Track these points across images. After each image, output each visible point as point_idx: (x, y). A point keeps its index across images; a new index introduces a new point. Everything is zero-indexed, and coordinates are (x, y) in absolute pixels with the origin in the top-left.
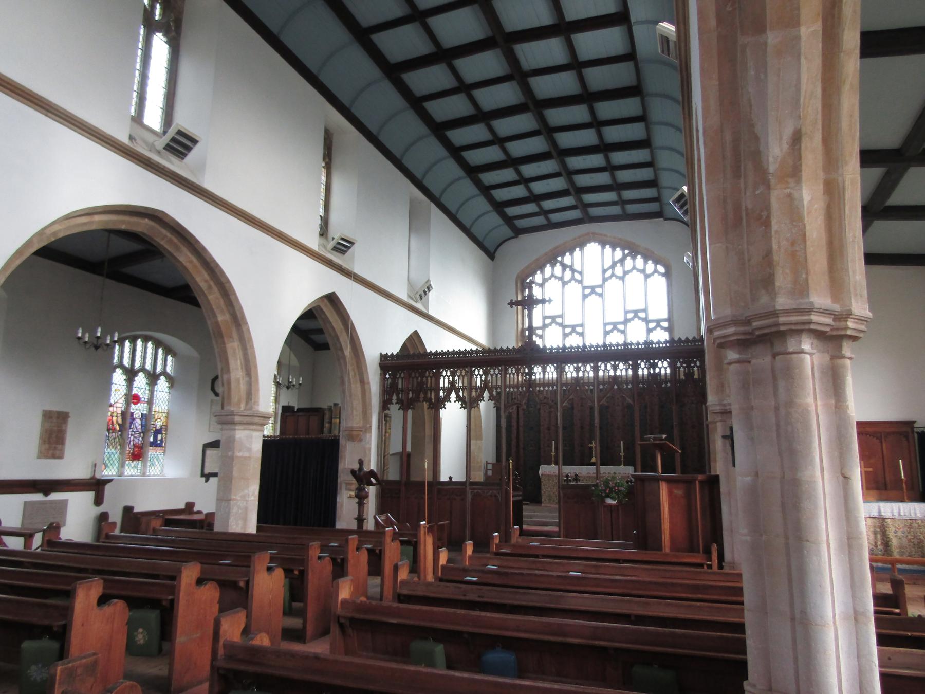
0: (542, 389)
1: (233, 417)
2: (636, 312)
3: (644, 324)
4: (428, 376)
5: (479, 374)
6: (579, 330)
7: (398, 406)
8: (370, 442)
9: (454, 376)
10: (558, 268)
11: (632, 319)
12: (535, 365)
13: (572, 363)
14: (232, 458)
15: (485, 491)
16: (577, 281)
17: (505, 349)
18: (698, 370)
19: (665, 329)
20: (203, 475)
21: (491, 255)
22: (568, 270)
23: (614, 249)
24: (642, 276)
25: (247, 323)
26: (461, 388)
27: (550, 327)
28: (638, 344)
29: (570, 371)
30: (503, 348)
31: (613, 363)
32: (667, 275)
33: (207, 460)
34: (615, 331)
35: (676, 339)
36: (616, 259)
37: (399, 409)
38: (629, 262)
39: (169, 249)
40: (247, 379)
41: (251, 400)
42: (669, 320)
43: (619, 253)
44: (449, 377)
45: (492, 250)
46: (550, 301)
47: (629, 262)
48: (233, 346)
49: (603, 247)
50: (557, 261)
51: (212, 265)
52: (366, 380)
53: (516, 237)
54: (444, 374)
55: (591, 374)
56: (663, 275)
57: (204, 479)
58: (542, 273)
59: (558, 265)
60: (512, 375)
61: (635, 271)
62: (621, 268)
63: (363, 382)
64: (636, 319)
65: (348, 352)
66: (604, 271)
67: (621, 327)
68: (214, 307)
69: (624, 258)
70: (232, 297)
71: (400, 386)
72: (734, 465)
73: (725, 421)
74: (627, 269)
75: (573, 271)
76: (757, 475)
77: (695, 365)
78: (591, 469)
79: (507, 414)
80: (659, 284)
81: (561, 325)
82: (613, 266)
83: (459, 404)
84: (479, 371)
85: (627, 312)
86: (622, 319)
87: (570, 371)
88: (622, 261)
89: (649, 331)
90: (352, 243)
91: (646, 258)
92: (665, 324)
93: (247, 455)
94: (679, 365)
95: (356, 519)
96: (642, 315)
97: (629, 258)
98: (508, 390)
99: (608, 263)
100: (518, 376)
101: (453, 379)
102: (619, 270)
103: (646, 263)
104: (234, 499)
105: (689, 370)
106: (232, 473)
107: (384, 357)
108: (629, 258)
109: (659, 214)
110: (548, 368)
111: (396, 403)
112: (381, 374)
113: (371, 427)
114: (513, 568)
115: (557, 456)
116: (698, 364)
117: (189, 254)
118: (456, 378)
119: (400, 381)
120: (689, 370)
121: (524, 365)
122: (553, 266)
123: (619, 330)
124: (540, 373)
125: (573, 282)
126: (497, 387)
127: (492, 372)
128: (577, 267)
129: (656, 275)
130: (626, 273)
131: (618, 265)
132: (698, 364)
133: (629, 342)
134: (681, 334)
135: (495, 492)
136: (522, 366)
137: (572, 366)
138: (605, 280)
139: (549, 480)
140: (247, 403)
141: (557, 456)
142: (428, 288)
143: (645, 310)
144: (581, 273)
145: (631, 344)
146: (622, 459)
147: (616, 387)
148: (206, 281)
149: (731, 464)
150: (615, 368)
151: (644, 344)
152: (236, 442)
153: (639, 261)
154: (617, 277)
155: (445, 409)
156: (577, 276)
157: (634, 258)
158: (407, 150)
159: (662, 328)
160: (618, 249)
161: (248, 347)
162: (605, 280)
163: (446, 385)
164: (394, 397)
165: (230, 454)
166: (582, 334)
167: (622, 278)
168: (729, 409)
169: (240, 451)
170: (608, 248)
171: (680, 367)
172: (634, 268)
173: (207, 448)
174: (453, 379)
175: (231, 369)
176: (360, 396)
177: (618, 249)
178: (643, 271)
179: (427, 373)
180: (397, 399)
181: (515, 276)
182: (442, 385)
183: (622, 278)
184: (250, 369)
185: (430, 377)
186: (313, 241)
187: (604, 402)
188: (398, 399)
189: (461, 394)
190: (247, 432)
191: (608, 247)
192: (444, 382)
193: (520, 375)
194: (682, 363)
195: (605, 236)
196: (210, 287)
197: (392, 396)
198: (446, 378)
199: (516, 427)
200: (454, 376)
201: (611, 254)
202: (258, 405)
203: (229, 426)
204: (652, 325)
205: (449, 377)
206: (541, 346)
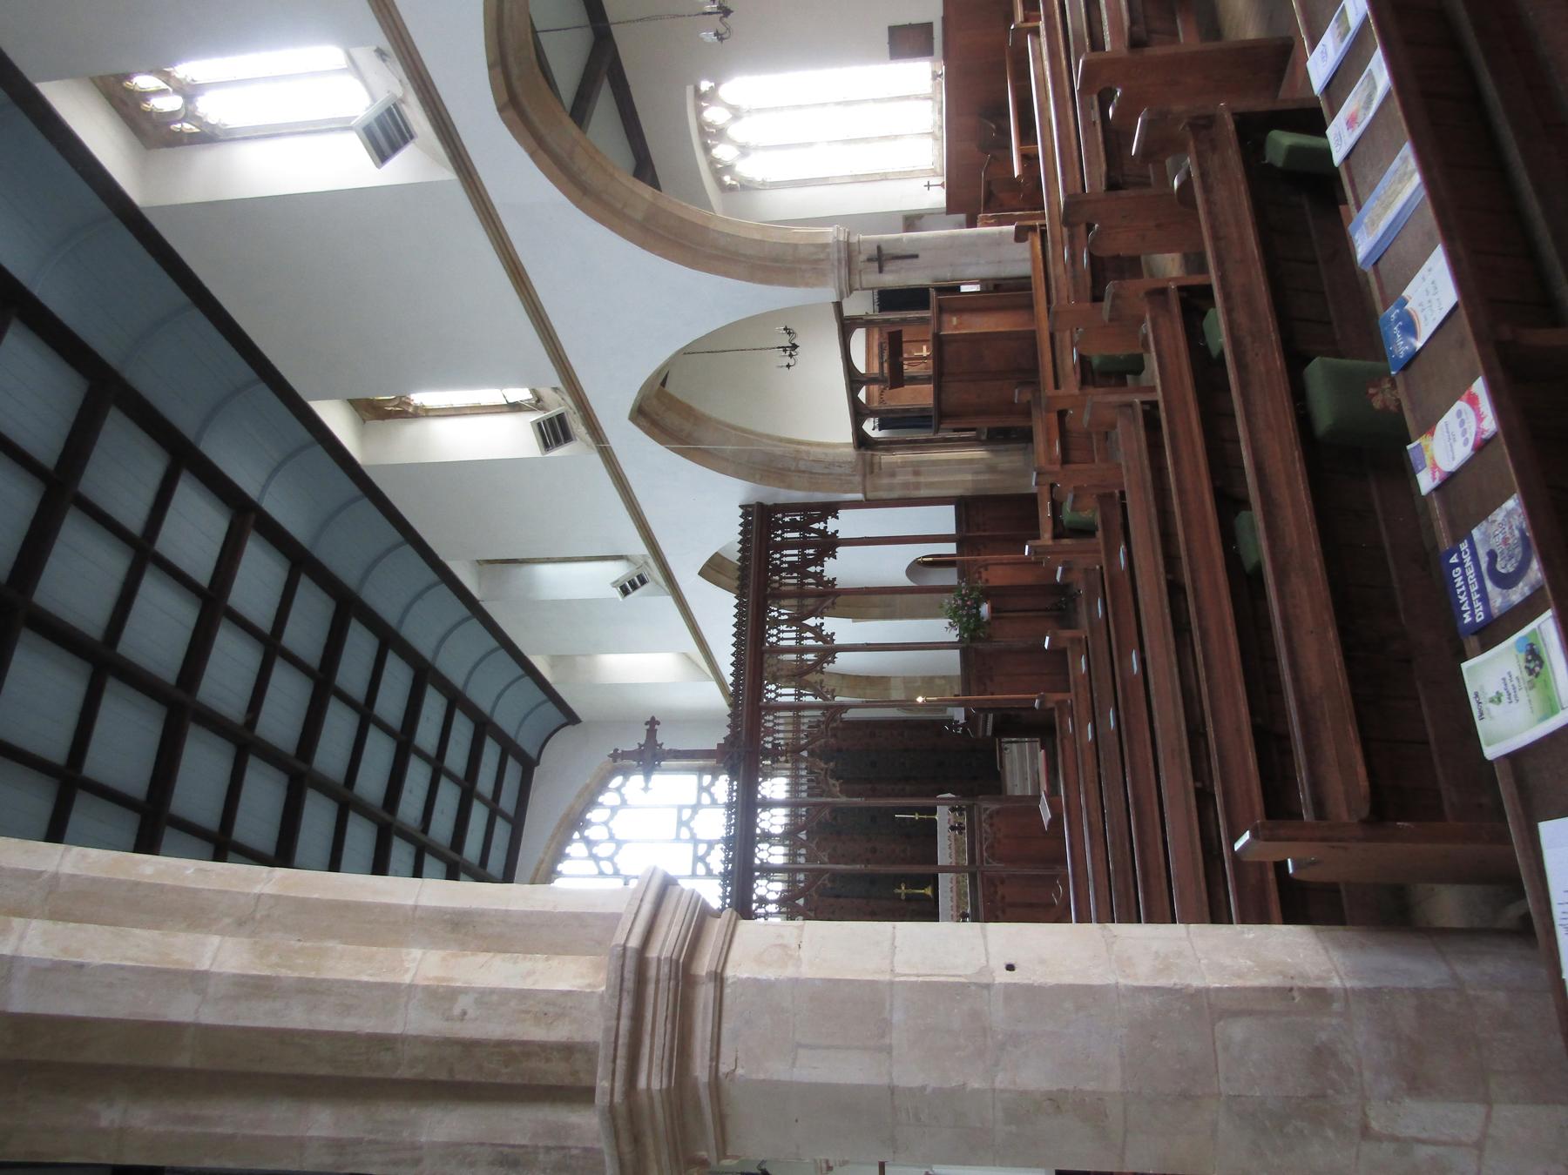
2: (681, 823)
3: (702, 812)
4: (779, 612)
5: (776, 635)
7: (831, 520)
11: (691, 830)
13: (764, 632)
15: (984, 835)
17: (735, 639)
18: (788, 516)
24: (621, 812)
26: (799, 691)
27: (695, 831)
29: (773, 854)
30: (740, 514)
31: (754, 906)
37: (837, 518)
43: (576, 849)
49: (560, 874)
54: (774, 639)
62: (602, 845)
64: (692, 824)
72: (916, 256)
73: (860, 271)
74: (606, 836)
77: (781, 519)
78: (945, 881)
82: (593, 857)
85: (678, 838)
88: (589, 843)
89: (714, 803)
91: (591, 803)
94: (779, 539)
96: (686, 814)
99: (591, 867)
100: (779, 732)
101: (784, 622)
102: (603, 850)
108: (587, 833)
109: (528, 765)
111: (826, 523)
115: (922, 810)
121: (760, 721)
124: (776, 717)
126: (800, 606)
129: (616, 859)
130: (612, 838)
132: (779, 516)
135: (984, 817)
136: (769, 563)
137: (761, 816)
138: (617, 873)
141: (922, 810)
146: (925, 817)
149: (915, 260)
150: (763, 901)
154: (616, 852)
155: (833, 634)
157: (588, 824)
158: (407, 609)
162: (617, 873)
163: (792, 691)
164: (816, 526)
167: (619, 844)
172: (606, 823)
174: (784, 622)
178: (614, 810)
179: (773, 614)
183: (619, 844)
185: (778, 633)
186: (604, 107)
187: (826, 860)
193: (777, 728)
195: (542, 862)
198: (781, 635)
204: (706, 799)
205: (780, 631)
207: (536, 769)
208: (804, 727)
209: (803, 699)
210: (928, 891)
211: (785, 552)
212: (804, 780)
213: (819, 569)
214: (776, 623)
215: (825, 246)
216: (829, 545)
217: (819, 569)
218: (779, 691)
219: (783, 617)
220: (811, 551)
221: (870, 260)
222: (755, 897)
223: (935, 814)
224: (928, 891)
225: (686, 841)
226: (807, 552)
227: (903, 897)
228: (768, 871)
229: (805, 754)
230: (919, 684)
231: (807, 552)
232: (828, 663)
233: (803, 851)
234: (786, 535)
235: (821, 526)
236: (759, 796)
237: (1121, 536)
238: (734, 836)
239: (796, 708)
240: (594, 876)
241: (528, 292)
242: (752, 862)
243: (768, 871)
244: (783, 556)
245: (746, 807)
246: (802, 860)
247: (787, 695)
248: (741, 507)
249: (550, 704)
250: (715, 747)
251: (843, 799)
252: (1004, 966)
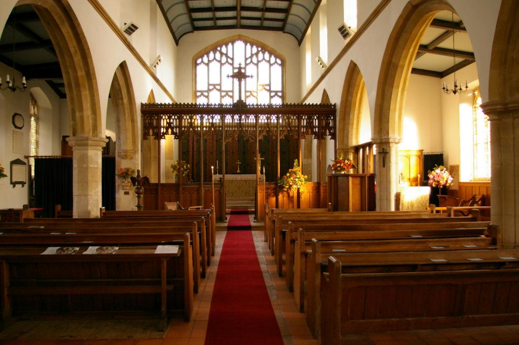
0: (247, 129)
1: (86, 141)
2: (214, 85)
3: (268, 93)
6: (231, 94)
8: (138, 160)
9: (170, 119)
10: (218, 55)
11: (213, 89)
12: (227, 114)
14: (87, 168)
16: (229, 63)
19: (280, 97)
20: (12, 183)
21: (177, 42)
22: (224, 56)
23: (252, 47)
25: (96, 78)
28: (215, 105)
29: (263, 119)
31: (211, 115)
32: (283, 65)
33: (14, 173)
34: (276, 96)
35: (285, 104)
36: (253, 53)
38: (261, 55)
39: (58, 23)
40: (94, 116)
41: (97, 130)
42: (282, 92)
43: (255, 50)
44: (167, 119)
45: (177, 37)
46: (228, 76)
47: (261, 55)
48: (85, 93)
50: (217, 50)
51: (81, 36)
52: (135, 120)
53: (192, 32)
54: (164, 117)
55: (276, 121)
56: (280, 65)
57: (12, 185)
58: (208, 57)
59: (218, 52)
60: (294, 120)
61: (264, 61)
63: (133, 121)
65: (125, 100)
66: (246, 59)
67: (206, 94)
68: (77, 66)
69: (258, 52)
70: (89, 60)
71: (155, 124)
72: (384, 166)
75: (227, 57)
76: (502, 164)
77: (154, 118)
79: (226, 143)
80: (277, 70)
81: (220, 90)
82: (252, 55)
83: (173, 136)
84: (305, 117)
85: (209, 85)
86: (206, 89)
87: (263, 119)
88: (257, 54)
90: (136, 28)
91: (271, 54)
92: (199, 94)
93: (96, 166)
94: (322, 118)
95: (137, 206)
96: (218, 87)
97: (261, 53)
98: (226, 129)
99: (248, 55)
102: (255, 59)
103: (270, 57)
104: (90, 195)
105: (151, 121)
106: (87, 179)
107: (142, 104)
108: (261, 53)
109: (281, 29)
110: (235, 116)
112: (142, 116)
113: (138, 150)
114: (322, 216)
116: (332, 118)
117: (68, 27)
118: (172, 121)
119: (155, 121)
120: (151, 121)
122: (215, 53)
123: (204, 96)
125: (227, 64)
127: (173, 117)
128: (230, 55)
131: (255, 56)
132: (332, 118)
133: (210, 104)
134: (290, 100)
138: (246, 65)
139: (232, 183)
140: (93, 133)
142: (160, 61)
143: (220, 85)
144: (232, 59)
145: (211, 105)
147: (213, 129)
148: (74, 47)
150: (213, 118)
151: (268, 105)
152: (89, 158)
153: (267, 55)
156: (230, 61)
159: (278, 96)
160: (255, 47)
161: (95, 95)
162: (246, 65)
163: (186, 125)
165: (85, 166)
166: (207, 97)
168: (386, 139)
169: (92, 164)
170: (249, 46)
171: (323, 120)
172: (215, 58)
173: (14, 165)
175: (84, 109)
176: (131, 130)
177: (255, 47)
178: (269, 62)
180: (172, 132)
181: (192, 57)
182: (162, 124)
184: (96, 109)
188: (153, 132)
189: (175, 130)
190: (95, 151)
191: (248, 44)
192: (164, 123)
194: (324, 117)
196: (76, 51)
197: (149, 131)
199: (192, 152)
200: (170, 119)
201: (251, 50)
202: (101, 134)
203: (82, 148)
204: (223, 94)
206: (244, 102)
207: (281, 32)
208: (249, 129)
209: (302, 129)
210: (238, 171)
211: (317, 120)
212: (228, 129)
213: (170, 133)
214: (170, 118)
215: (388, 133)
216: (321, 137)
217: (170, 133)
218: (305, 120)
219: (291, 120)
220: (317, 130)
221: (383, 149)
222: (214, 115)
223: (219, 174)
224: (238, 171)
225: (208, 88)
226: (317, 128)
227: (236, 163)
228: (223, 118)
229: (240, 129)
230: (309, 169)
231: (317, 128)
232: (315, 137)
233: (236, 129)
234: (155, 120)
235: (328, 134)
236: (260, 115)
237: (167, 241)
238: (272, 107)
239: (299, 126)
240: (245, 56)
241: (385, 4)
242: (259, 114)
243: (223, 118)
244: (315, 120)
245: (269, 110)
246: (226, 129)
247: (304, 123)
248: (335, 104)
249: (301, 35)
250: (242, 99)
251: (224, 144)
252: (399, 191)
